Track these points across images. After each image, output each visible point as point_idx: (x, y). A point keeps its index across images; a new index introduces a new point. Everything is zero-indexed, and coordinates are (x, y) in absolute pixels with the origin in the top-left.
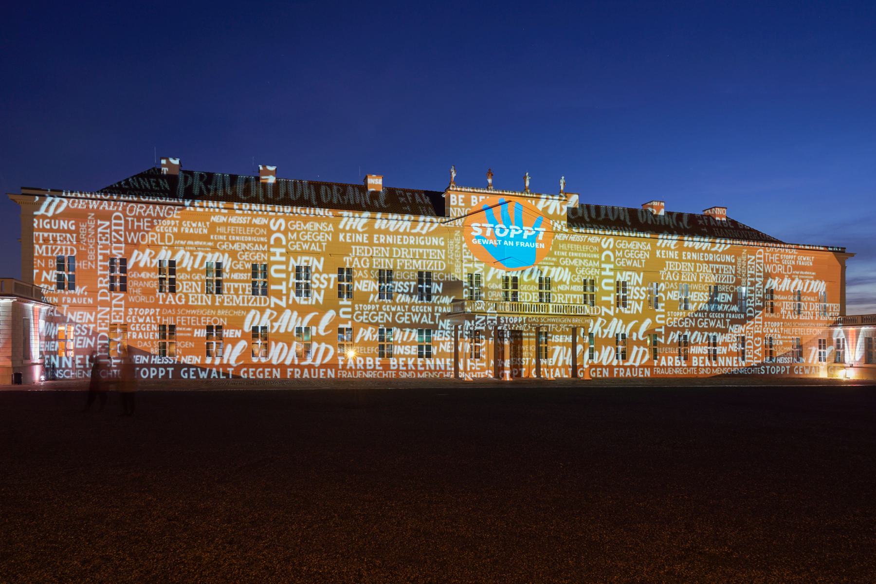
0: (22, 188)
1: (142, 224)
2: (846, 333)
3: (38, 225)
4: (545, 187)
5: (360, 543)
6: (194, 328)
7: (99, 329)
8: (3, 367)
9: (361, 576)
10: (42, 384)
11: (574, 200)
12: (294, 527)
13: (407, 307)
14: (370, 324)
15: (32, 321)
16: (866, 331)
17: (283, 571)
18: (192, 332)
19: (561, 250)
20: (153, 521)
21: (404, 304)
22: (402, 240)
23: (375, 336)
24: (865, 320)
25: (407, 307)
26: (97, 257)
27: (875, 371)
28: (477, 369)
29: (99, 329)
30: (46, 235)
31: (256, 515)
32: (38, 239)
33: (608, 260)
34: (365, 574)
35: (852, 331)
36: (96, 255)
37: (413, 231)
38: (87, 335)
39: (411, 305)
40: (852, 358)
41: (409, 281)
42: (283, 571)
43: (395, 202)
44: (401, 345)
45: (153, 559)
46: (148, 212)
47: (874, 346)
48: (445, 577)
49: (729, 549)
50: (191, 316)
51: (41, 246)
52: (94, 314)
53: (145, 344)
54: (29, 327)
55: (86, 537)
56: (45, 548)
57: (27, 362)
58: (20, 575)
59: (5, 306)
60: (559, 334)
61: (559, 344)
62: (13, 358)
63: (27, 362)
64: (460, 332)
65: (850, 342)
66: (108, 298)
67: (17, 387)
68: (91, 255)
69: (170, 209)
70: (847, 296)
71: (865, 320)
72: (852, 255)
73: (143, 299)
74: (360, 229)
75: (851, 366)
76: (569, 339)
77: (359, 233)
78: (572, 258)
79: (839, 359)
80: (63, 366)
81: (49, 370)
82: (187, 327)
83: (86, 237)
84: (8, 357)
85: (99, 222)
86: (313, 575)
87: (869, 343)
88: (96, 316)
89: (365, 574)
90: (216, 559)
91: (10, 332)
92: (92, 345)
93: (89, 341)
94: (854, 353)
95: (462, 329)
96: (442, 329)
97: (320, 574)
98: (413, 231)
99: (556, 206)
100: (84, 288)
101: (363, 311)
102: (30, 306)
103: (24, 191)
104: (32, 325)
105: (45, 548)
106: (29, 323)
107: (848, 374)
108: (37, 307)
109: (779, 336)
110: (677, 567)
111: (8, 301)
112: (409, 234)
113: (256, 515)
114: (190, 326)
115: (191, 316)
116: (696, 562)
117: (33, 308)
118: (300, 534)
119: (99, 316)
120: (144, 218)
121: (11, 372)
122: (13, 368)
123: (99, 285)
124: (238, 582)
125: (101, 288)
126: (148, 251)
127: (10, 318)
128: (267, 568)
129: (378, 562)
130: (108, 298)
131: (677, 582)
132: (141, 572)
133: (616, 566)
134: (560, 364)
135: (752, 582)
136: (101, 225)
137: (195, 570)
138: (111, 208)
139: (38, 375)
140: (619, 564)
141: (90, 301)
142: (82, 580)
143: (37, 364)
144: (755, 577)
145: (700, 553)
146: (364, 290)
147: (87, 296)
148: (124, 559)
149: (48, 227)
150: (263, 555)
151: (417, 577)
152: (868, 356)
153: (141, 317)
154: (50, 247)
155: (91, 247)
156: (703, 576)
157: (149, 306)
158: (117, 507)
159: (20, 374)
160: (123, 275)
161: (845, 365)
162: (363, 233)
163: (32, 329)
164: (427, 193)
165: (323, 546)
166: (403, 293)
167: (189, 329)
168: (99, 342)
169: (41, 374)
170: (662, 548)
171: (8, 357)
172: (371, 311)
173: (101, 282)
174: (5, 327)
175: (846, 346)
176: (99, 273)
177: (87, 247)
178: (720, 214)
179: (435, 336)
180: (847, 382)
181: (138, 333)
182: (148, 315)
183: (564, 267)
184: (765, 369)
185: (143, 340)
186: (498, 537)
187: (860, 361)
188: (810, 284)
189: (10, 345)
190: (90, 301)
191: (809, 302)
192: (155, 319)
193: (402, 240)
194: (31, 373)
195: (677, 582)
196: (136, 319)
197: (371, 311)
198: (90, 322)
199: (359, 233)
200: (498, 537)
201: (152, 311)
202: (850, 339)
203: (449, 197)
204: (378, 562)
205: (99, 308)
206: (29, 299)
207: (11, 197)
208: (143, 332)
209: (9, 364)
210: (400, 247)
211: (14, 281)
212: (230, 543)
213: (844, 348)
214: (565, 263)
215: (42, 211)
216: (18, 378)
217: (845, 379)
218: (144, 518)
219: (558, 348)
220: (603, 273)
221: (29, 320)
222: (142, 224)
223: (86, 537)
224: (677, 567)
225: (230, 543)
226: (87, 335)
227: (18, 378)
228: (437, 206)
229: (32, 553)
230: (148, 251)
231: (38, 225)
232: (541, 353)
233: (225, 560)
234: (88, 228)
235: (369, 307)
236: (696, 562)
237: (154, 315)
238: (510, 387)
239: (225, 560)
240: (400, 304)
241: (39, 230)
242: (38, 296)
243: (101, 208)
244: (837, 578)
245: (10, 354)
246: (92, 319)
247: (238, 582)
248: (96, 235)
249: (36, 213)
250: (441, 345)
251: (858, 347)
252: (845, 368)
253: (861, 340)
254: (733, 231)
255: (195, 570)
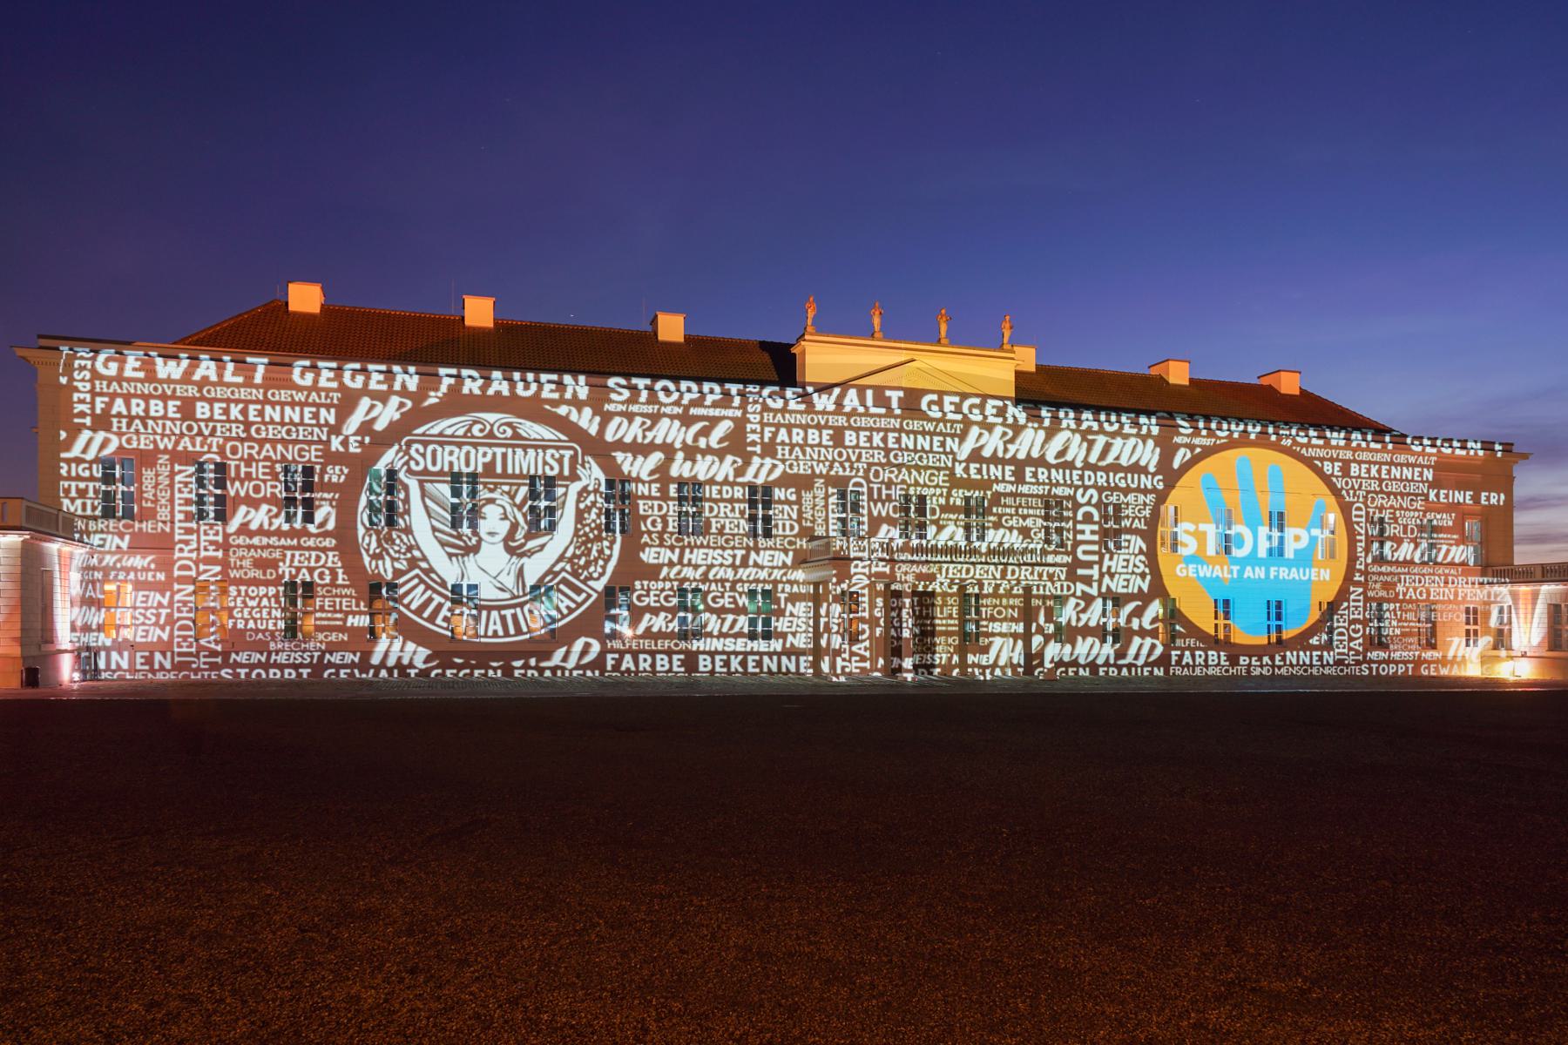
0: (40, 337)
1: (253, 470)
2: (1515, 596)
3: (69, 472)
4: (976, 335)
5: (645, 972)
6: (347, 614)
7: (176, 615)
8: (5, 657)
9: (646, 1031)
10: (75, 686)
11: (1027, 358)
12: (525, 943)
13: (728, 585)
14: (663, 609)
15: (57, 575)
16: (1550, 594)
17: (506, 1022)
18: (345, 620)
19: (1005, 506)
20: (274, 933)
21: (723, 581)
22: (720, 492)
23: (671, 626)
24: (1549, 573)
25: (728, 585)
26: (173, 516)
27: (1567, 664)
28: (853, 663)
29: (176, 615)
30: (82, 485)
31: (459, 921)
32: (67, 491)
33: (1088, 518)
34: (653, 1027)
35: (1526, 593)
36: (172, 512)
37: (740, 480)
38: (156, 624)
39: (734, 583)
40: (1525, 642)
41: (733, 548)
42: (506, 1022)
43: (704, 360)
44: (718, 637)
45: (274, 1000)
46: (264, 453)
47: (1564, 619)
48: (796, 1032)
49: (1304, 982)
50: (341, 596)
51: (73, 500)
52: (168, 594)
53: (260, 636)
54: (52, 585)
55: (153, 961)
56: (80, 981)
57: (49, 648)
58: (35, 1029)
59: (9, 549)
60: (1001, 621)
61: (1001, 635)
62: (23, 641)
63: (49, 648)
64: (823, 620)
65: (1521, 611)
66: (193, 573)
67: (30, 693)
68: (163, 513)
69: (301, 450)
70: (1516, 531)
71: (1549, 573)
72: (1525, 456)
73: (258, 574)
74: (644, 477)
75: (1524, 655)
76: (1020, 628)
77: (643, 482)
78: (1024, 517)
79: (1501, 639)
80: (113, 666)
81: (87, 657)
82: (335, 611)
83: (155, 487)
84: (14, 639)
85: (177, 468)
86: (561, 1029)
87: (1555, 612)
88: (172, 597)
89: (653, 1027)
90: (386, 1001)
91: (17, 595)
92: (165, 637)
93: (158, 632)
94: (1529, 632)
95: (827, 615)
96: (792, 615)
97: (572, 1027)
98: (740, 480)
99: (997, 371)
100: (150, 558)
101: (649, 590)
102: (54, 547)
103: (43, 342)
104: (57, 582)
105: (80, 981)
106: (52, 578)
107: (1519, 668)
108: (67, 549)
109: (1394, 623)
110: (1213, 1015)
111: (13, 539)
112: (733, 484)
113: (459, 921)
114: (341, 611)
115: (341, 596)
116: (1245, 1005)
117: (59, 551)
118: (537, 956)
119: (177, 597)
120: (257, 461)
121: (19, 666)
122: (24, 658)
123: (177, 555)
124: (426, 1041)
125: (179, 619)
126: (265, 507)
127: (18, 570)
128: (477, 1016)
129: (677, 1006)
130: (193, 573)
131: (1213, 1041)
132: (253, 1023)
133: (1103, 1013)
134: (1002, 662)
135: (1346, 1042)
136: (180, 472)
137: (350, 1020)
138: (198, 449)
139: (67, 672)
140: (1108, 1011)
141: (161, 576)
142: (146, 1038)
143: (66, 651)
144: (1351, 1032)
145: (1253, 990)
146: (652, 561)
147: (155, 571)
148: (222, 1000)
149: (87, 474)
150: (471, 993)
151: (746, 1033)
152: (1554, 639)
153: (252, 598)
154: (89, 502)
155: (163, 501)
156: (1259, 1031)
157: (267, 583)
158: (210, 907)
159: (35, 671)
160: (218, 492)
161: (1513, 654)
162: (650, 482)
163: (58, 590)
164: (764, 346)
165: (578, 977)
166: (721, 565)
167: (339, 616)
168: (176, 633)
169: (74, 670)
170: (1185, 981)
171: (14, 639)
172: (663, 590)
173: (181, 550)
174: (9, 586)
175: (1514, 619)
176: (177, 538)
177: (155, 501)
178: (1289, 385)
179: (779, 624)
180: (1517, 684)
181: (247, 621)
182: (266, 595)
183: (1011, 529)
184: (1370, 669)
185: (257, 631)
186: (890, 961)
187: (1539, 645)
188: (1448, 551)
189: (18, 618)
190: (161, 576)
191: (1446, 575)
192: (278, 602)
193: (720, 492)
194: (56, 669)
195: (1213, 1041)
196: (244, 602)
197: (663, 590)
198: (160, 605)
199: (643, 482)
200: (890, 961)
201: (272, 591)
202: (1521, 606)
203: (803, 353)
204: (677, 1006)
205: (176, 587)
206: (51, 535)
207: (20, 352)
208: (259, 610)
209: (16, 651)
210: (716, 501)
211: (25, 503)
212: (412, 971)
213: (1510, 623)
214: (1013, 523)
215: (76, 451)
216: (32, 676)
217: (1512, 679)
218: (257, 927)
219: (998, 641)
220: (1079, 537)
221: (51, 572)
222: (253, 470)
223: (153, 961)
224: (1213, 1015)
225: (413, 971)
226: (156, 624)
227: (32, 676)
228: (781, 367)
229: (58, 990)
230: (265, 507)
231: (69, 472)
232: (970, 641)
233: (402, 1003)
234: (157, 475)
235: (660, 585)
236: (1245, 1005)
237: (276, 596)
238: (911, 692)
239: (402, 1003)
240: (716, 581)
241: (69, 478)
242: (65, 528)
243: (180, 448)
244: (1498, 1034)
245: (18, 634)
246: (165, 602)
247: (426, 1041)
248: (171, 486)
249: (64, 455)
250: (790, 637)
251: (1536, 620)
252: (1512, 658)
253: (1541, 608)
254: (1316, 413)
255: (350, 1020)
